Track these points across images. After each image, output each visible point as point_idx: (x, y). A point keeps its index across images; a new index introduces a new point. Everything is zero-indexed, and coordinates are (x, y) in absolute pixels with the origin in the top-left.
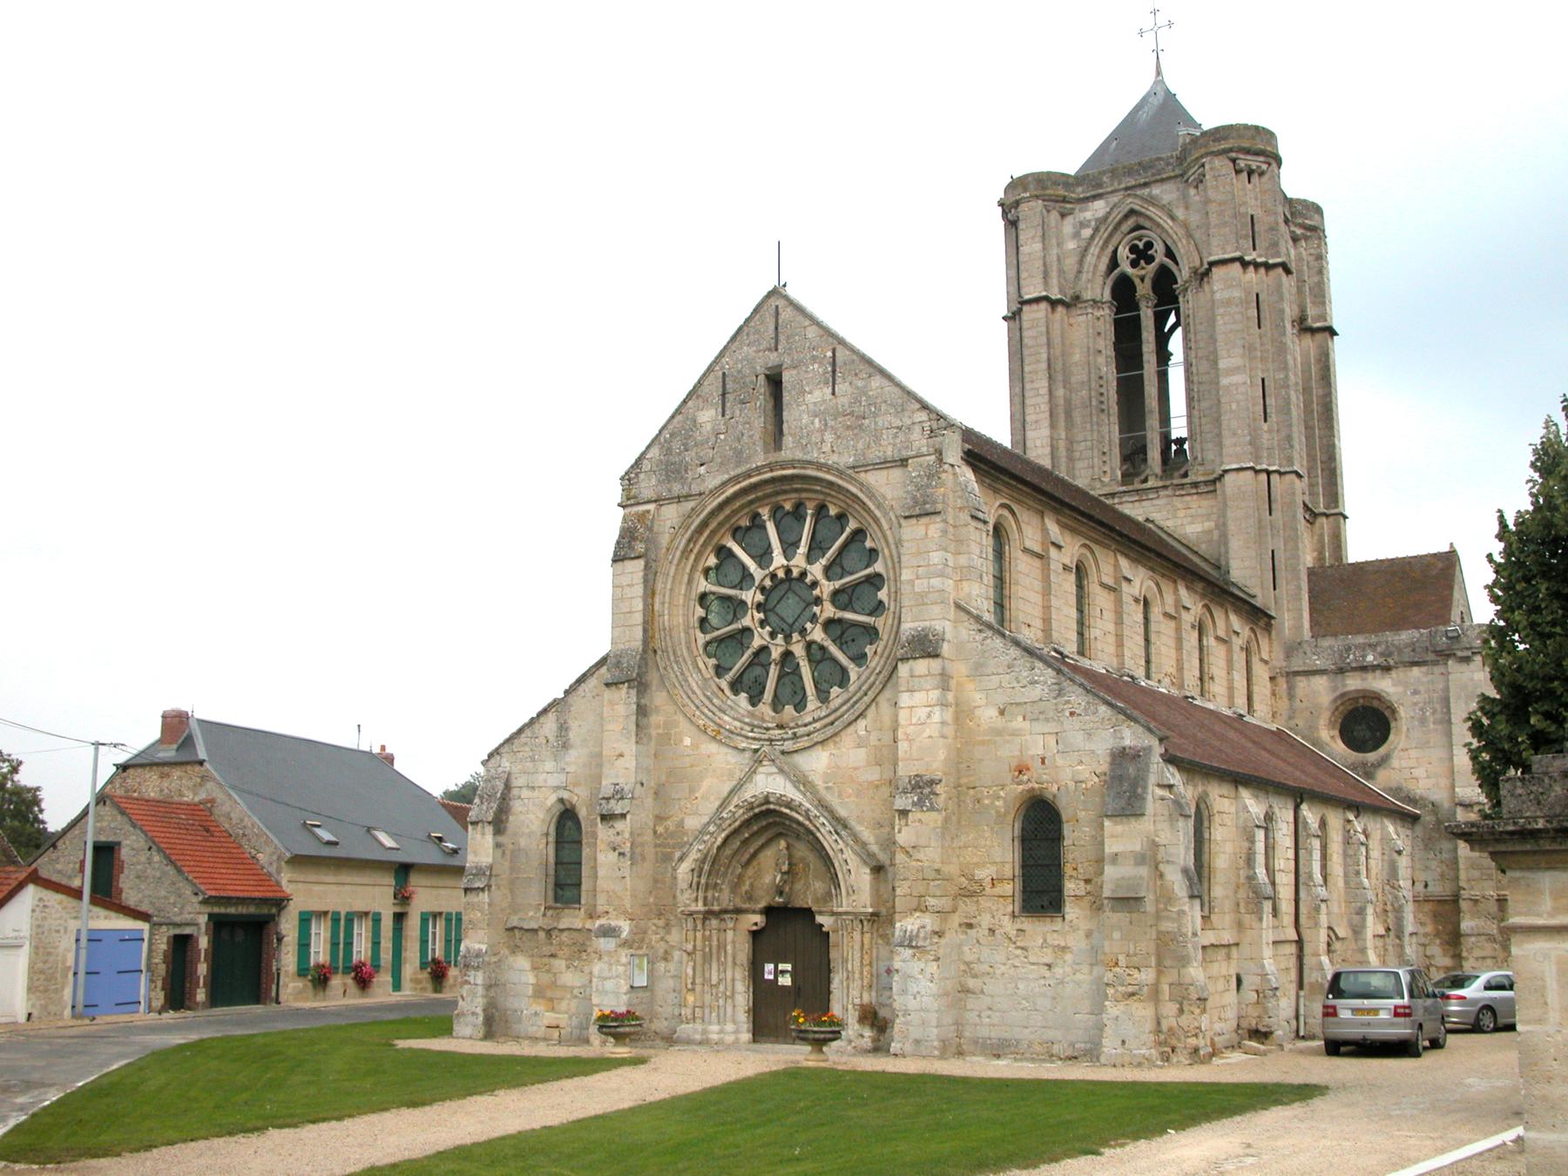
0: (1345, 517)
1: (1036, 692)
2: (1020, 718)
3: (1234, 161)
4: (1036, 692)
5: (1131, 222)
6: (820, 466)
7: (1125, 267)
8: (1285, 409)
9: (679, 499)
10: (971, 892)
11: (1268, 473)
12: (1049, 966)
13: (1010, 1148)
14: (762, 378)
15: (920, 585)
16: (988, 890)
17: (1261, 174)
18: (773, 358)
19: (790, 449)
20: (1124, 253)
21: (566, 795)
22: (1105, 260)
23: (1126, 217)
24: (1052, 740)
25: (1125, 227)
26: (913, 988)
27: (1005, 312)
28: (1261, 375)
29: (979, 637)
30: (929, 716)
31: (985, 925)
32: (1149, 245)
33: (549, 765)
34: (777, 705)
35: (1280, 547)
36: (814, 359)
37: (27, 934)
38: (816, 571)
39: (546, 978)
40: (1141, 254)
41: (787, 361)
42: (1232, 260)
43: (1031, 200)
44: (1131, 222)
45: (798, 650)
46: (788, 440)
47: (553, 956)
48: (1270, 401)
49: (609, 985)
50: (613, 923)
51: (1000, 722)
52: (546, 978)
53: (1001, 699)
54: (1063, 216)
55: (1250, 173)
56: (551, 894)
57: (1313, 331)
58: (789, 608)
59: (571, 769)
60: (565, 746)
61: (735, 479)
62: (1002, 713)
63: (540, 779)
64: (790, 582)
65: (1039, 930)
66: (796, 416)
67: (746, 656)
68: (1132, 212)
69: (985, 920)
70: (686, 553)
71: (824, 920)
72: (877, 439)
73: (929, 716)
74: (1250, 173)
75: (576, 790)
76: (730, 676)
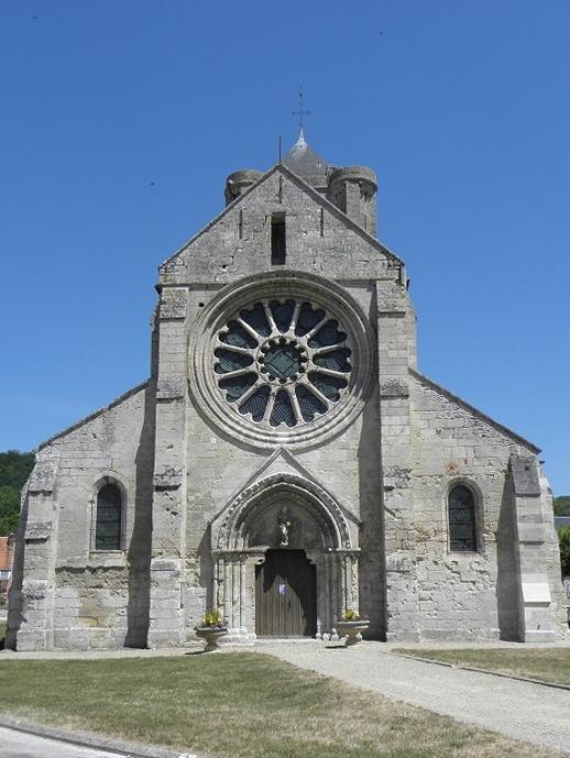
1: (460, 422)
2: (450, 437)
4: (460, 422)
6: (313, 277)
9: (207, 287)
10: (424, 537)
12: (474, 583)
13: (238, 686)
14: (269, 219)
15: (392, 354)
16: (432, 538)
18: (279, 208)
19: (291, 264)
21: (111, 474)
24: (471, 451)
26: (401, 597)
29: (422, 388)
30: (402, 431)
31: (431, 559)
33: (96, 454)
34: (308, 417)
36: (309, 212)
38: (303, 341)
39: (91, 603)
41: (289, 210)
45: (291, 388)
46: (289, 259)
47: (100, 587)
49: (165, 604)
50: (166, 560)
51: (438, 439)
52: (91, 603)
53: (438, 424)
56: (93, 543)
58: (283, 361)
59: (117, 456)
60: (111, 440)
61: (250, 279)
62: (439, 432)
63: (88, 463)
64: (283, 347)
65: (467, 560)
66: (292, 245)
67: (340, 373)
69: (431, 556)
70: (211, 321)
71: (313, 557)
72: (353, 266)
73: (402, 431)
75: (120, 471)
76: (239, 401)
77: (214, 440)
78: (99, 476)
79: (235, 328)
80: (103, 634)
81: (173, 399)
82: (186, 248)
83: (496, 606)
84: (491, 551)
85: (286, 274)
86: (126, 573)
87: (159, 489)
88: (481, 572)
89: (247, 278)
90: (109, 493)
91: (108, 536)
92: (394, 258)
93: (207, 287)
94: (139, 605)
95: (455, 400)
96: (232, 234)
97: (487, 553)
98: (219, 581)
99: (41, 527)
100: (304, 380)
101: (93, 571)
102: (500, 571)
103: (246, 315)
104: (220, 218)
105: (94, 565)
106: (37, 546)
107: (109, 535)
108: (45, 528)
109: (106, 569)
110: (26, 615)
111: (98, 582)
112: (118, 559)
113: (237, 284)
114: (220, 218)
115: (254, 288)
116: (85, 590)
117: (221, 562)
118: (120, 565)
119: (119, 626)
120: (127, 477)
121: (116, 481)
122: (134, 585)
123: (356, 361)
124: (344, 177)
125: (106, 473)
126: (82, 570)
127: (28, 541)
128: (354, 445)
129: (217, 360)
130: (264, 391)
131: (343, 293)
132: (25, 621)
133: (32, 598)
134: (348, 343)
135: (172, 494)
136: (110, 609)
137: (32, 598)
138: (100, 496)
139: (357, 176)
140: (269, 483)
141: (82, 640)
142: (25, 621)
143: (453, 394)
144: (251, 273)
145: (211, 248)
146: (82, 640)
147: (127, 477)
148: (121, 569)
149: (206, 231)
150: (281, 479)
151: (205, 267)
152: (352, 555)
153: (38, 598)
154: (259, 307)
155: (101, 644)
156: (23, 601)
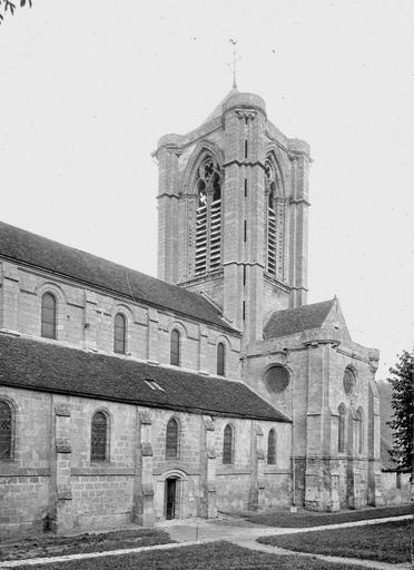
0: (309, 205)
3: (237, 112)
5: (204, 154)
7: (203, 177)
8: (255, 236)
11: (245, 265)
17: (253, 119)
20: (203, 170)
22: (194, 175)
23: (202, 151)
25: (202, 157)
27: (157, 195)
28: (244, 219)
32: (212, 165)
35: (248, 299)
37: (61, 342)
40: (209, 170)
42: (232, 163)
43: (169, 148)
44: (204, 154)
48: (248, 231)
54: (178, 155)
55: (247, 119)
57: (297, 203)
68: (204, 149)
74: (247, 119)
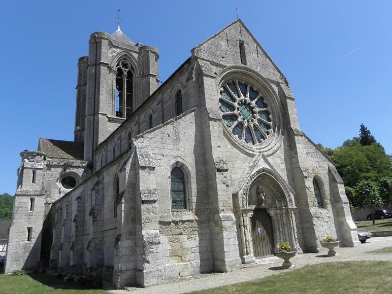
9: (218, 65)
21: (181, 160)
33: (171, 147)
39: (176, 246)
47: (181, 234)
52: (176, 246)
60: (178, 139)
63: (166, 152)
71: (272, 212)
77: (229, 147)
78: (173, 161)
79: (226, 90)
80: (186, 267)
81: (217, 119)
82: (205, 42)
83: (335, 232)
84: (330, 207)
85: (245, 68)
86: (195, 224)
87: (219, 170)
88: (329, 217)
89: (232, 67)
90: (178, 172)
91: (180, 202)
92: (283, 76)
93: (218, 65)
94: (204, 245)
95: (310, 141)
96: (224, 43)
97: (329, 209)
98: (244, 226)
99: (150, 192)
100: (256, 122)
101: (176, 223)
102: (334, 216)
103: (229, 84)
104: (218, 34)
105: (178, 219)
106: (150, 206)
107: (178, 199)
108: (154, 193)
109: (183, 222)
110: (149, 258)
111: (178, 231)
112: (189, 215)
113: (230, 68)
114: (218, 34)
115: (234, 72)
116: (171, 236)
117: (244, 215)
118: (191, 219)
119: (194, 260)
120: (189, 162)
121: (183, 165)
122: (200, 232)
123: (274, 116)
124: (148, 49)
125: (178, 159)
126: (169, 223)
127: (144, 202)
128: (282, 156)
129: (220, 104)
130: (240, 125)
131: (269, 85)
132: (148, 262)
133: (152, 243)
134: (269, 109)
135: (225, 174)
136: (188, 249)
137: (152, 243)
138: (172, 173)
139: (154, 50)
140: (258, 172)
141: (174, 272)
142: (148, 262)
143: (309, 138)
144: (234, 65)
145: (216, 47)
146: (174, 272)
147: (189, 162)
148: (191, 221)
149: (213, 37)
150: (263, 170)
151: (215, 55)
152: (293, 209)
153: (156, 244)
154: (234, 83)
155: (186, 274)
156: (145, 247)
